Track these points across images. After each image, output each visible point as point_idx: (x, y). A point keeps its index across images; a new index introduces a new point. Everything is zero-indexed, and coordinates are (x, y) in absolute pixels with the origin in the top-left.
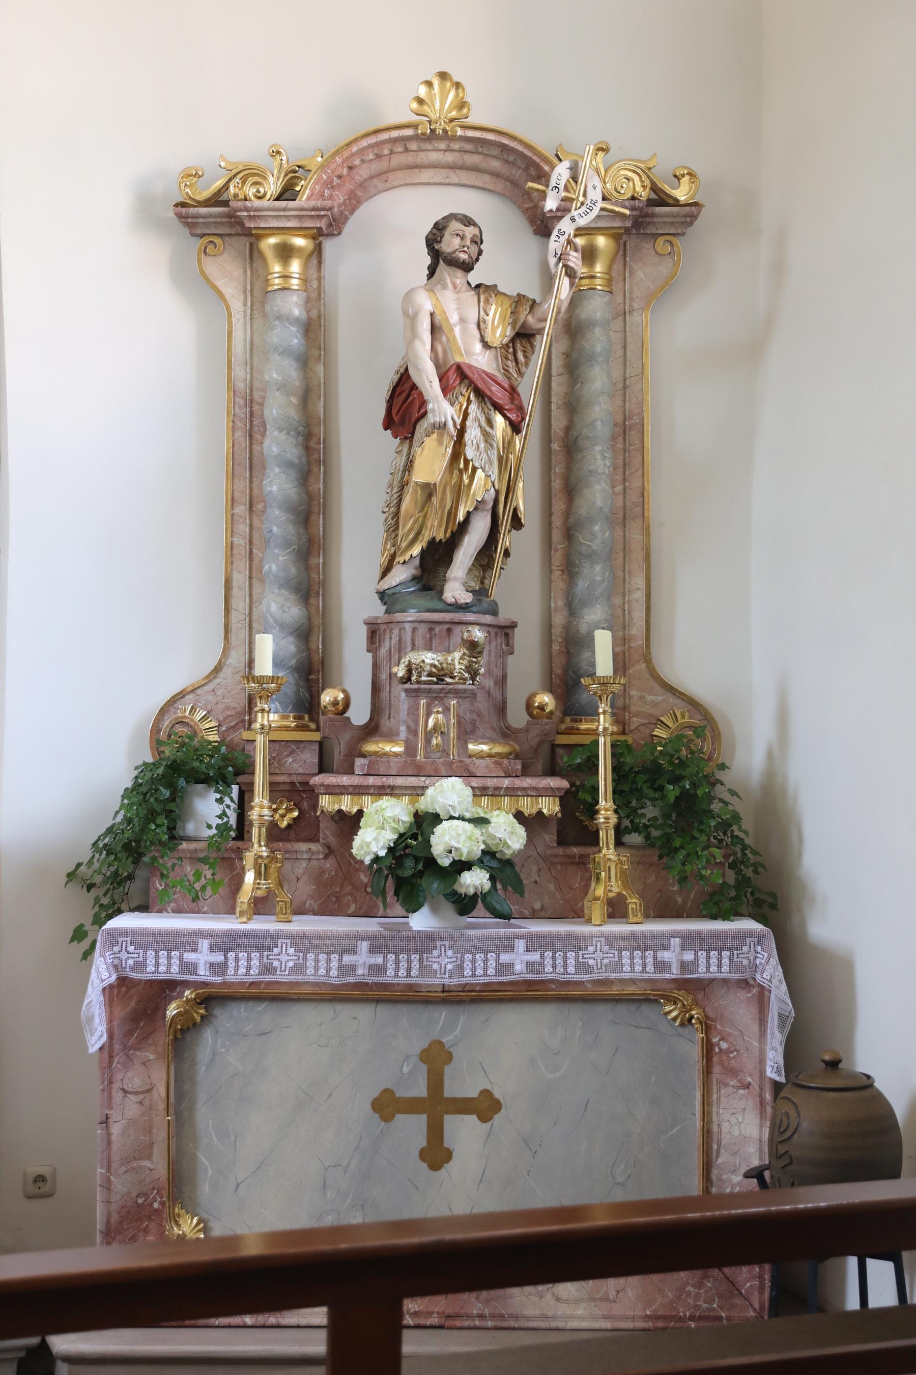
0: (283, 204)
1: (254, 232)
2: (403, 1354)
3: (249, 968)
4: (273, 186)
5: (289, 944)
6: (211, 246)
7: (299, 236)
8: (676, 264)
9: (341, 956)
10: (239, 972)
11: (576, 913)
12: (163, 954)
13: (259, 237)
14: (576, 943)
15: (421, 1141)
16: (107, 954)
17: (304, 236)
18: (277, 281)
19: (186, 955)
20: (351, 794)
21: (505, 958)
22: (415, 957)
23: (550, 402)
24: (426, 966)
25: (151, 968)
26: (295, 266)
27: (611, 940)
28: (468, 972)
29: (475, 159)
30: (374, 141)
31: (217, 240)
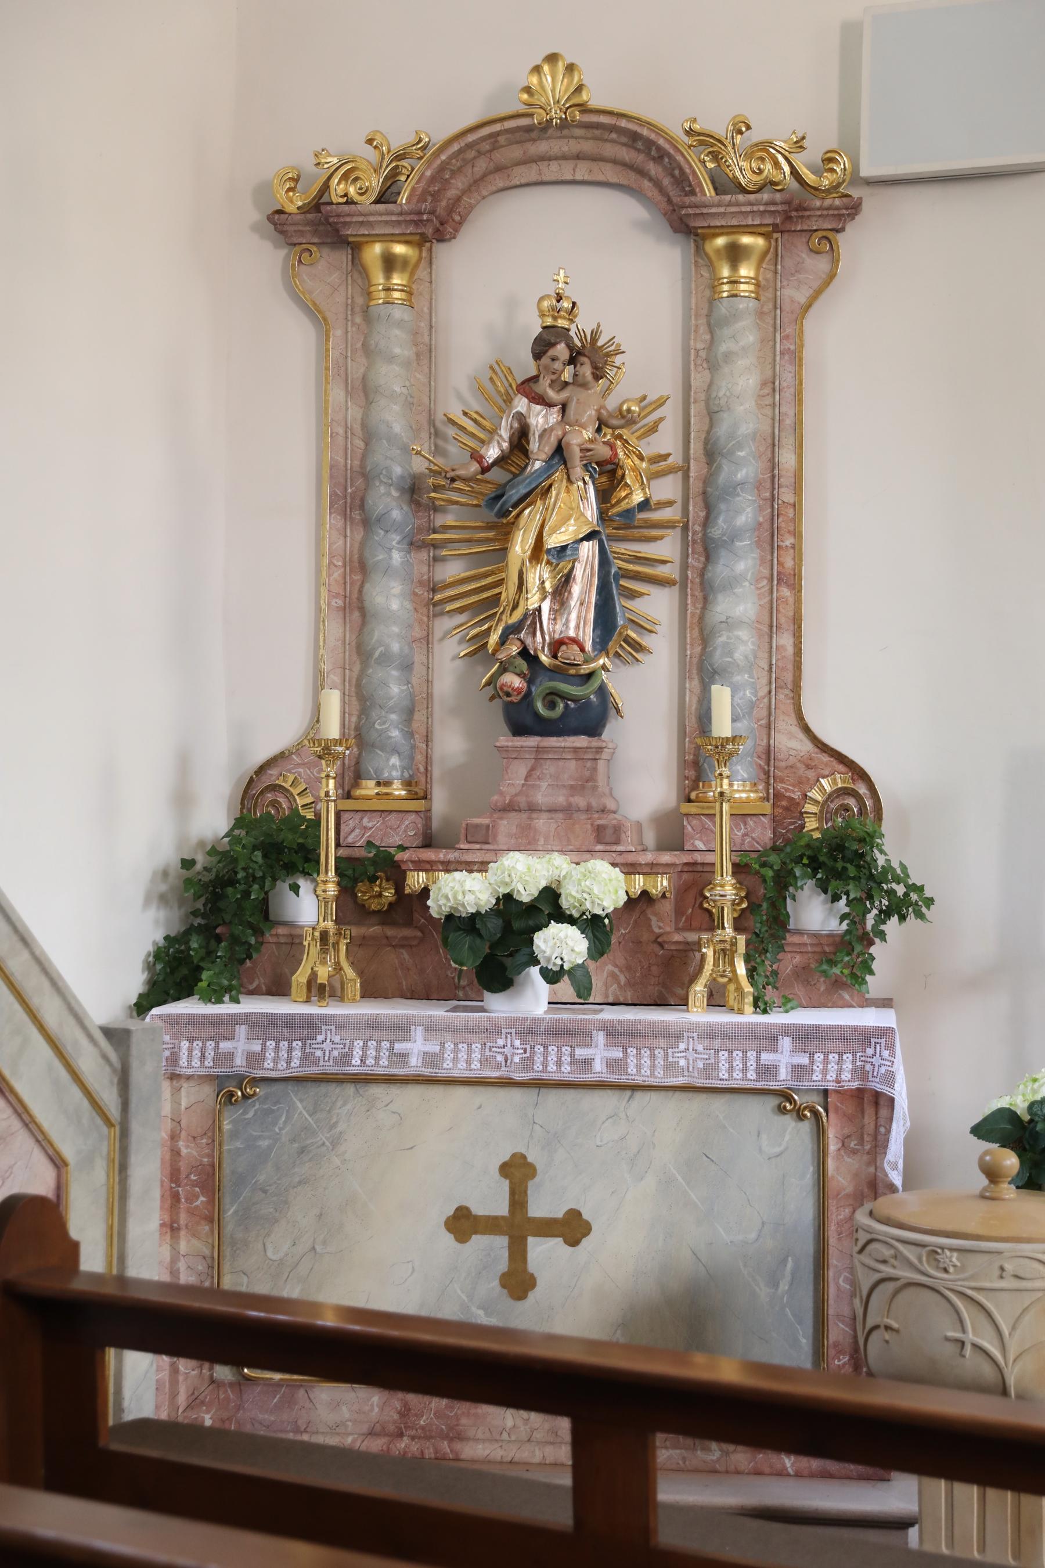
0: (380, 207)
1: (351, 239)
2: (659, 1466)
3: (289, 1060)
4: (375, 183)
5: (883, 1045)
6: (306, 255)
7: (399, 242)
8: (835, 261)
9: (759, 1053)
10: (292, 1064)
11: (683, 1002)
12: (284, 1045)
13: (704, 238)
14: (672, 1035)
15: (555, 1244)
16: (859, 1054)
17: (407, 242)
18: (726, 287)
19: (397, 1046)
20: (643, 874)
21: (766, 1057)
22: (297, 1044)
23: (689, 434)
24: (671, 1064)
25: (356, 1061)
26: (746, 271)
27: (711, 1034)
28: (538, 1067)
29: (587, 147)
30: (515, 125)
31: (314, 248)
